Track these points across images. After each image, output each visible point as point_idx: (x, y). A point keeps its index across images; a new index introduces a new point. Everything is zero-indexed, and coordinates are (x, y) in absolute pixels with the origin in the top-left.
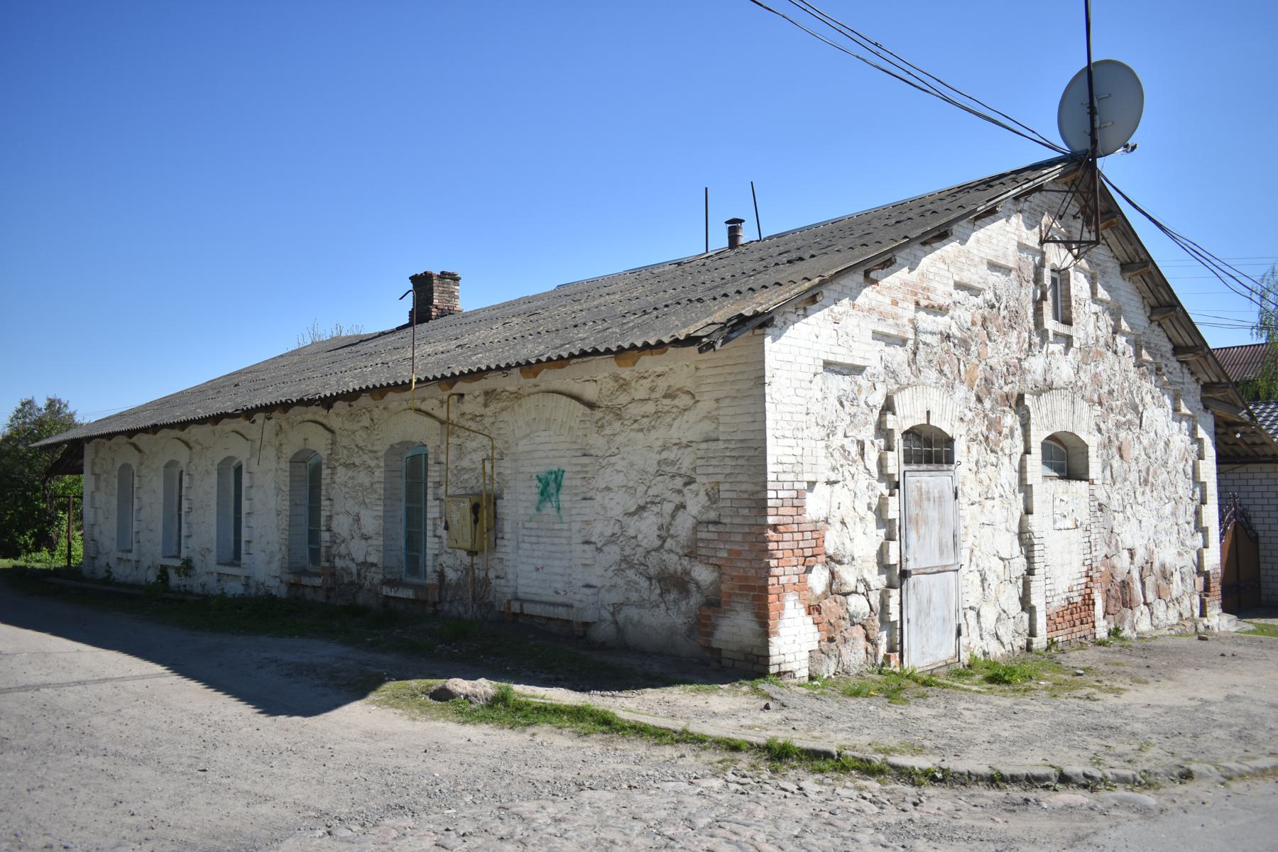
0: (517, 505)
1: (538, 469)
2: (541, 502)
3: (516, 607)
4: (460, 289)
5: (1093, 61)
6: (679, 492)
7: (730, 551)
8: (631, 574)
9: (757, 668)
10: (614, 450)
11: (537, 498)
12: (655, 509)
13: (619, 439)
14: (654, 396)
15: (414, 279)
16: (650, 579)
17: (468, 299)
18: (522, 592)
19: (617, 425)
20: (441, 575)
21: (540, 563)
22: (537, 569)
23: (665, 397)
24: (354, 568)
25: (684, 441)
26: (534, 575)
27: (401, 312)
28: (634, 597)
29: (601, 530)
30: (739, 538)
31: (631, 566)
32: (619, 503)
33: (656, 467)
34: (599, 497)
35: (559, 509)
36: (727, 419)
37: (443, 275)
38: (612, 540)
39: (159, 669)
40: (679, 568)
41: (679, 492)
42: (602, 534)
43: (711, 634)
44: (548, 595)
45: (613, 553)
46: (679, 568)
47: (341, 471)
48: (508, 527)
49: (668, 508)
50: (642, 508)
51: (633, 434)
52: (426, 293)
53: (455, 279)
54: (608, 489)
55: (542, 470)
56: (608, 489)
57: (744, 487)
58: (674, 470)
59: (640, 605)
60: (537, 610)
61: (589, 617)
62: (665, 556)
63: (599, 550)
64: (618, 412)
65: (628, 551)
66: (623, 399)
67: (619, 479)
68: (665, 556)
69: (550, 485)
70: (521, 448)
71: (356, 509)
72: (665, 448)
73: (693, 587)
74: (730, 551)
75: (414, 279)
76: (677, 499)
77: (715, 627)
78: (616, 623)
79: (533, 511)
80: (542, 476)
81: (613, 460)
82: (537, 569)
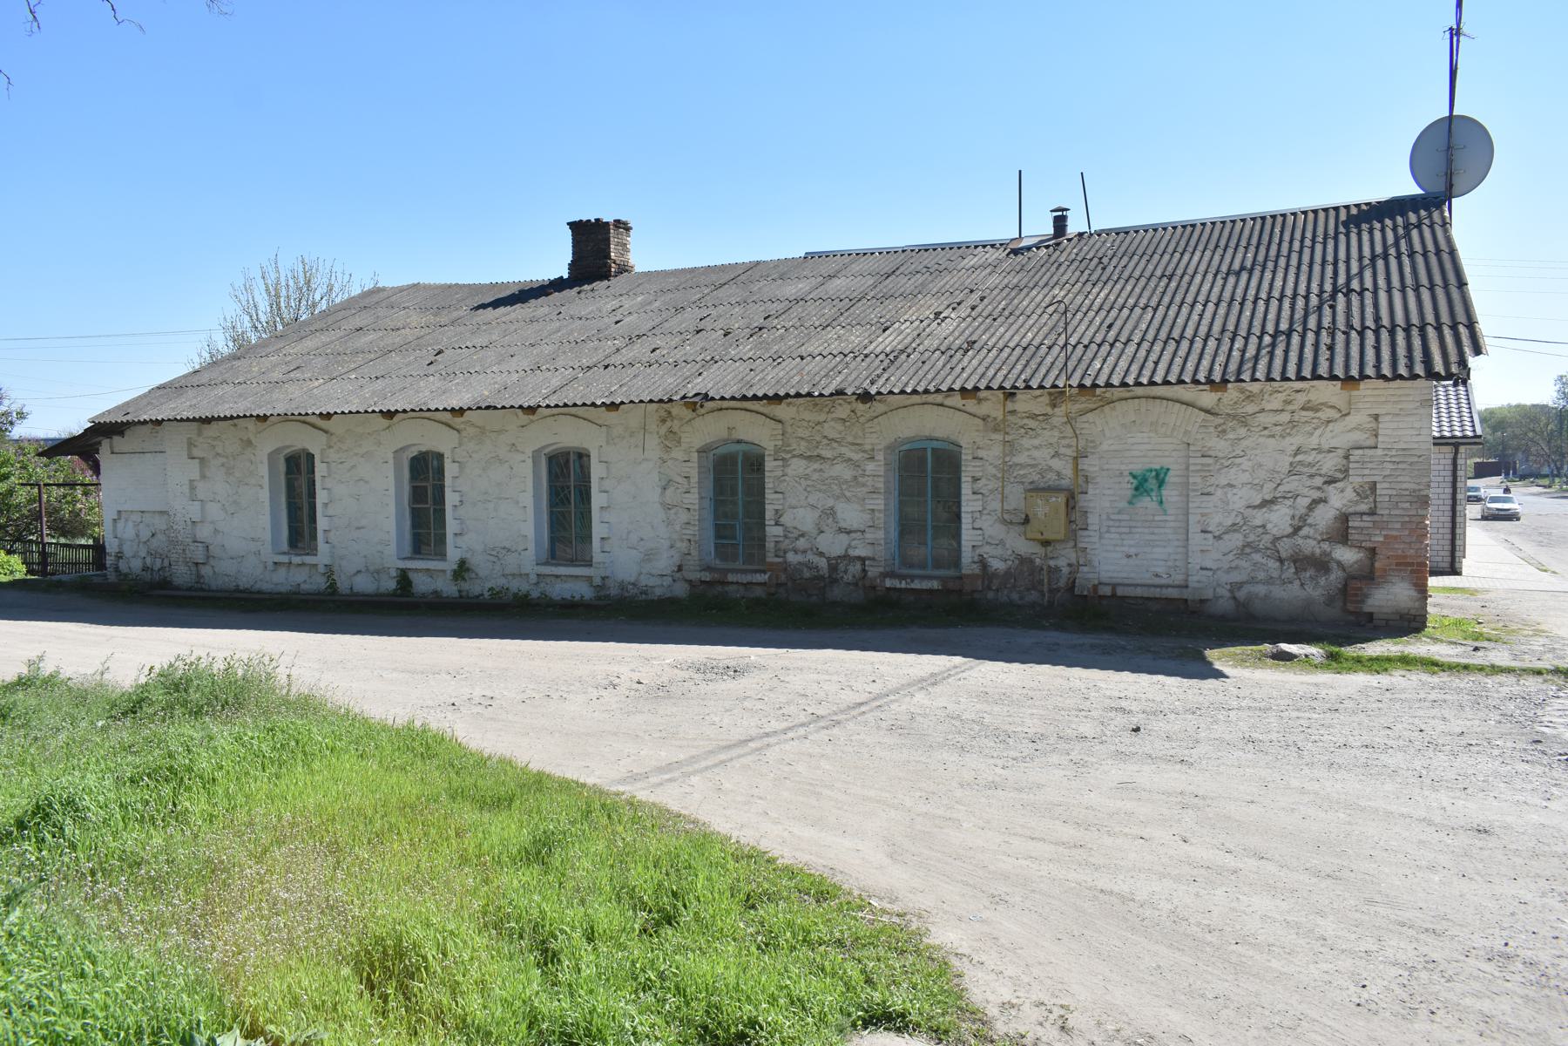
0: (1103, 499)
1: (1131, 466)
2: (1134, 496)
3: (1107, 591)
4: (633, 240)
5: (1455, 113)
6: (1319, 488)
7: (1386, 536)
8: (1257, 557)
9: (1414, 625)
10: (1239, 452)
11: (1130, 493)
12: (1288, 503)
13: (1244, 443)
14: (1290, 407)
15: (578, 228)
16: (1281, 561)
17: (644, 253)
18: (1105, 577)
19: (1242, 431)
20: (983, 563)
21: (1132, 551)
22: (1129, 556)
23: (1303, 409)
24: (823, 563)
25: (1326, 447)
26: (1125, 561)
27: (557, 263)
28: (1261, 575)
29: (1217, 521)
30: (1398, 526)
31: (1257, 550)
32: (1240, 498)
33: (1288, 468)
34: (1219, 492)
35: (1161, 502)
36: (1389, 432)
37: (617, 222)
38: (1234, 528)
39: (958, 660)
40: (1318, 551)
41: (1319, 488)
42: (1220, 524)
43: (1363, 602)
44: (1147, 578)
45: (1236, 540)
46: (1318, 551)
47: (797, 466)
48: (1093, 520)
49: (1303, 502)
50: (1273, 501)
51: (1262, 440)
52: (594, 249)
53: (628, 229)
54: (1232, 486)
55: (1138, 467)
56: (1232, 486)
57: (1405, 486)
58: (1313, 471)
59: (1270, 581)
60: (1139, 592)
61: (1209, 594)
62: (1300, 541)
63: (1218, 538)
64: (1243, 421)
65: (1252, 538)
66: (1251, 408)
67: (1245, 477)
68: (1300, 541)
69: (1147, 483)
70: (1105, 447)
71: (830, 503)
72: (1298, 451)
73: (1334, 566)
74: (1386, 536)
75: (578, 228)
76: (1316, 495)
77: (1367, 596)
78: (1234, 598)
79: (1123, 504)
80: (1138, 473)
81: (1238, 461)
82: (1129, 556)
